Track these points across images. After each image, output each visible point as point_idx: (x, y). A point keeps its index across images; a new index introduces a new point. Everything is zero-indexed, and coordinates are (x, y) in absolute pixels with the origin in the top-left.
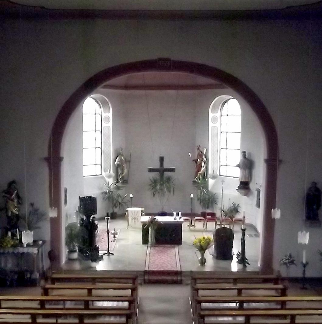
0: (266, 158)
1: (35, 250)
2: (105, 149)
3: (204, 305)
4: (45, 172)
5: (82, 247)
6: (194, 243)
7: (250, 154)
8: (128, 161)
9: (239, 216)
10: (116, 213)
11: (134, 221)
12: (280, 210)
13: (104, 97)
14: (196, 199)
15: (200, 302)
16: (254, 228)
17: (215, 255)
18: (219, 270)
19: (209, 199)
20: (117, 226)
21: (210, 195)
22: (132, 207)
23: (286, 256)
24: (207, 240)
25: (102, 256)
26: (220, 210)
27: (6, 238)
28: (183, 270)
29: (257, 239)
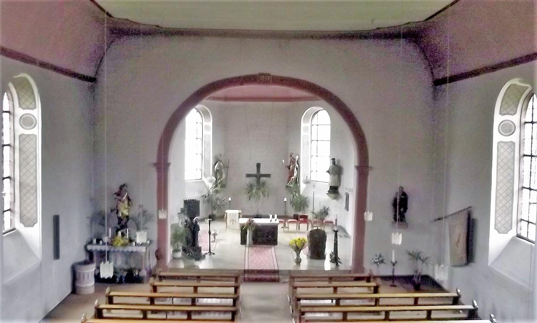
0: (356, 164)
1: (143, 249)
2: (206, 155)
3: (303, 302)
4: (154, 174)
5: (186, 246)
6: (290, 244)
7: (339, 161)
8: (227, 167)
9: (328, 219)
10: (214, 215)
11: (232, 222)
12: (372, 213)
13: (205, 107)
14: (289, 202)
15: (299, 299)
16: (344, 231)
17: (309, 255)
18: (314, 269)
19: (301, 203)
20: (217, 226)
21: (302, 199)
22: (230, 209)
23: (376, 256)
24: (302, 241)
25: (204, 256)
26: (311, 213)
27: (117, 238)
28: (280, 269)
29: (347, 240)
